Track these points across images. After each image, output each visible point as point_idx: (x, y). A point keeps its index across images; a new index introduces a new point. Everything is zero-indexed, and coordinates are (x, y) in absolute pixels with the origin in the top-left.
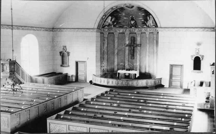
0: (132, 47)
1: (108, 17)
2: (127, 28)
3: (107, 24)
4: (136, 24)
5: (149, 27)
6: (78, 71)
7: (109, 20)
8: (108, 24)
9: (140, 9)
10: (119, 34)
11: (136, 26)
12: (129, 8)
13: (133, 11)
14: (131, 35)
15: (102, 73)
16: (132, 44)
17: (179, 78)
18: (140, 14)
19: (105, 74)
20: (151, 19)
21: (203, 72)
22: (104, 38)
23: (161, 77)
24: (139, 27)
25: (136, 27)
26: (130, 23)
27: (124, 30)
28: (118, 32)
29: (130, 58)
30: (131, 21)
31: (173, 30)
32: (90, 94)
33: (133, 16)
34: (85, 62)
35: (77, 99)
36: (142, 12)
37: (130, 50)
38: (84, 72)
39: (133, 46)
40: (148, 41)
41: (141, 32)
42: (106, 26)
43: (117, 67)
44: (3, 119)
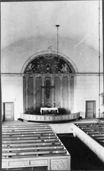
2: (43, 73)
4: (51, 70)
5: (63, 72)
6: (5, 111)
11: (50, 72)
12: (48, 57)
14: (47, 79)
15: (25, 112)
17: (92, 111)
19: (27, 111)
20: (65, 67)
24: (54, 72)
25: (51, 73)
28: (36, 76)
34: (12, 103)
41: (55, 76)
42: (27, 71)
44: (62, 161)
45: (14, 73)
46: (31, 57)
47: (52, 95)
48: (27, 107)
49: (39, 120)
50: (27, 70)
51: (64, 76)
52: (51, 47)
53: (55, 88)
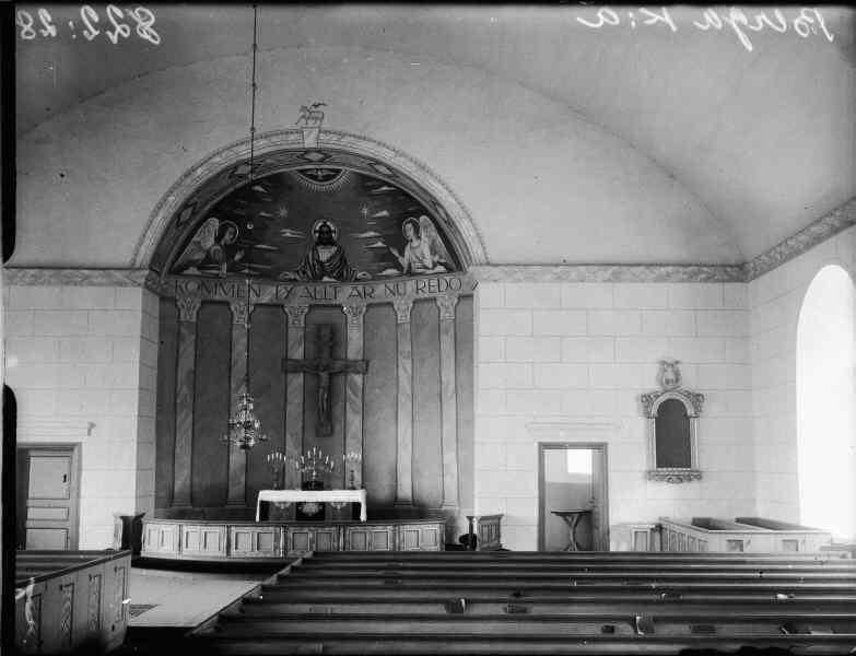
0: (324, 375)
1: (205, 219)
2: (295, 279)
3: (196, 257)
4: (343, 261)
5: (410, 273)
7: (207, 238)
8: (199, 256)
9: (369, 184)
10: (258, 310)
11: (341, 271)
12: (315, 178)
13: (331, 194)
14: (320, 316)
16: (324, 363)
21: (704, 475)
23: (499, 513)
24: (359, 275)
25: (340, 277)
26: (313, 259)
27: (283, 292)
28: (254, 299)
30: (319, 248)
31: (548, 277)
32: (149, 607)
33: (328, 223)
35: (93, 628)
36: (376, 203)
37: (310, 394)
38: (61, 503)
39: (327, 368)
40: (405, 347)
42: (191, 263)
43: (243, 479)
45: (88, 264)
46: (199, 171)
47: (350, 415)
48: (182, 481)
49: (193, 552)
50: (191, 257)
51: (421, 295)
52: (316, 106)
53: (365, 372)
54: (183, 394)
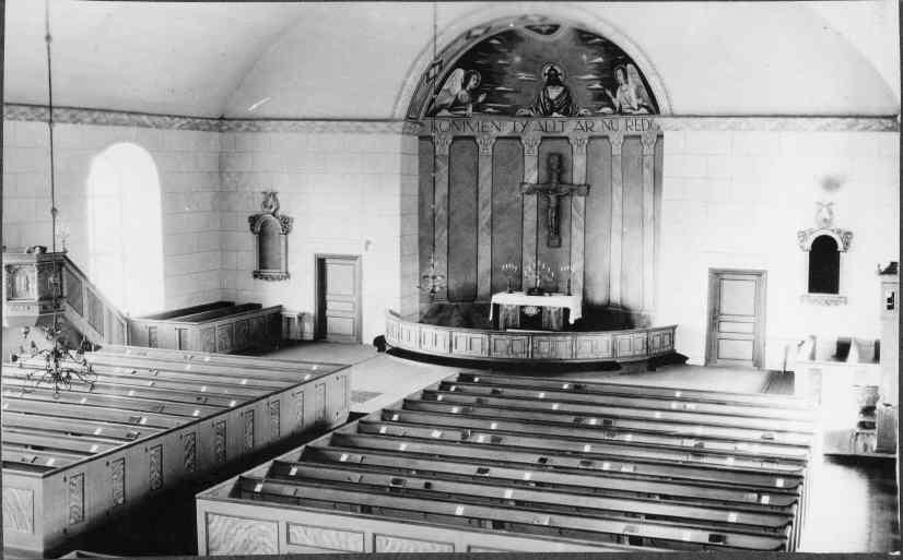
0: (553, 198)
1: (452, 70)
2: (529, 116)
3: (446, 101)
4: (569, 100)
5: (621, 112)
6: (328, 297)
7: (456, 85)
8: (449, 100)
9: (585, 36)
10: (499, 141)
11: (567, 107)
12: (539, 31)
13: (555, 44)
14: (549, 147)
15: (426, 307)
16: (554, 185)
17: (748, 328)
18: (585, 57)
19: (441, 308)
20: (630, 79)
21: (849, 300)
22: (435, 157)
23: (673, 324)
24: (582, 112)
25: (567, 113)
26: (544, 98)
27: (520, 127)
28: (495, 133)
29: (543, 241)
30: (549, 89)
31: (724, 126)
32: (374, 395)
33: (556, 68)
34: (354, 258)
35: (321, 415)
36: (594, 51)
37: (542, 211)
38: (350, 299)
39: (555, 191)
40: (617, 173)
41: (589, 133)
42: (443, 107)
43: (489, 280)
44: (14, 496)
54: (436, 226)
